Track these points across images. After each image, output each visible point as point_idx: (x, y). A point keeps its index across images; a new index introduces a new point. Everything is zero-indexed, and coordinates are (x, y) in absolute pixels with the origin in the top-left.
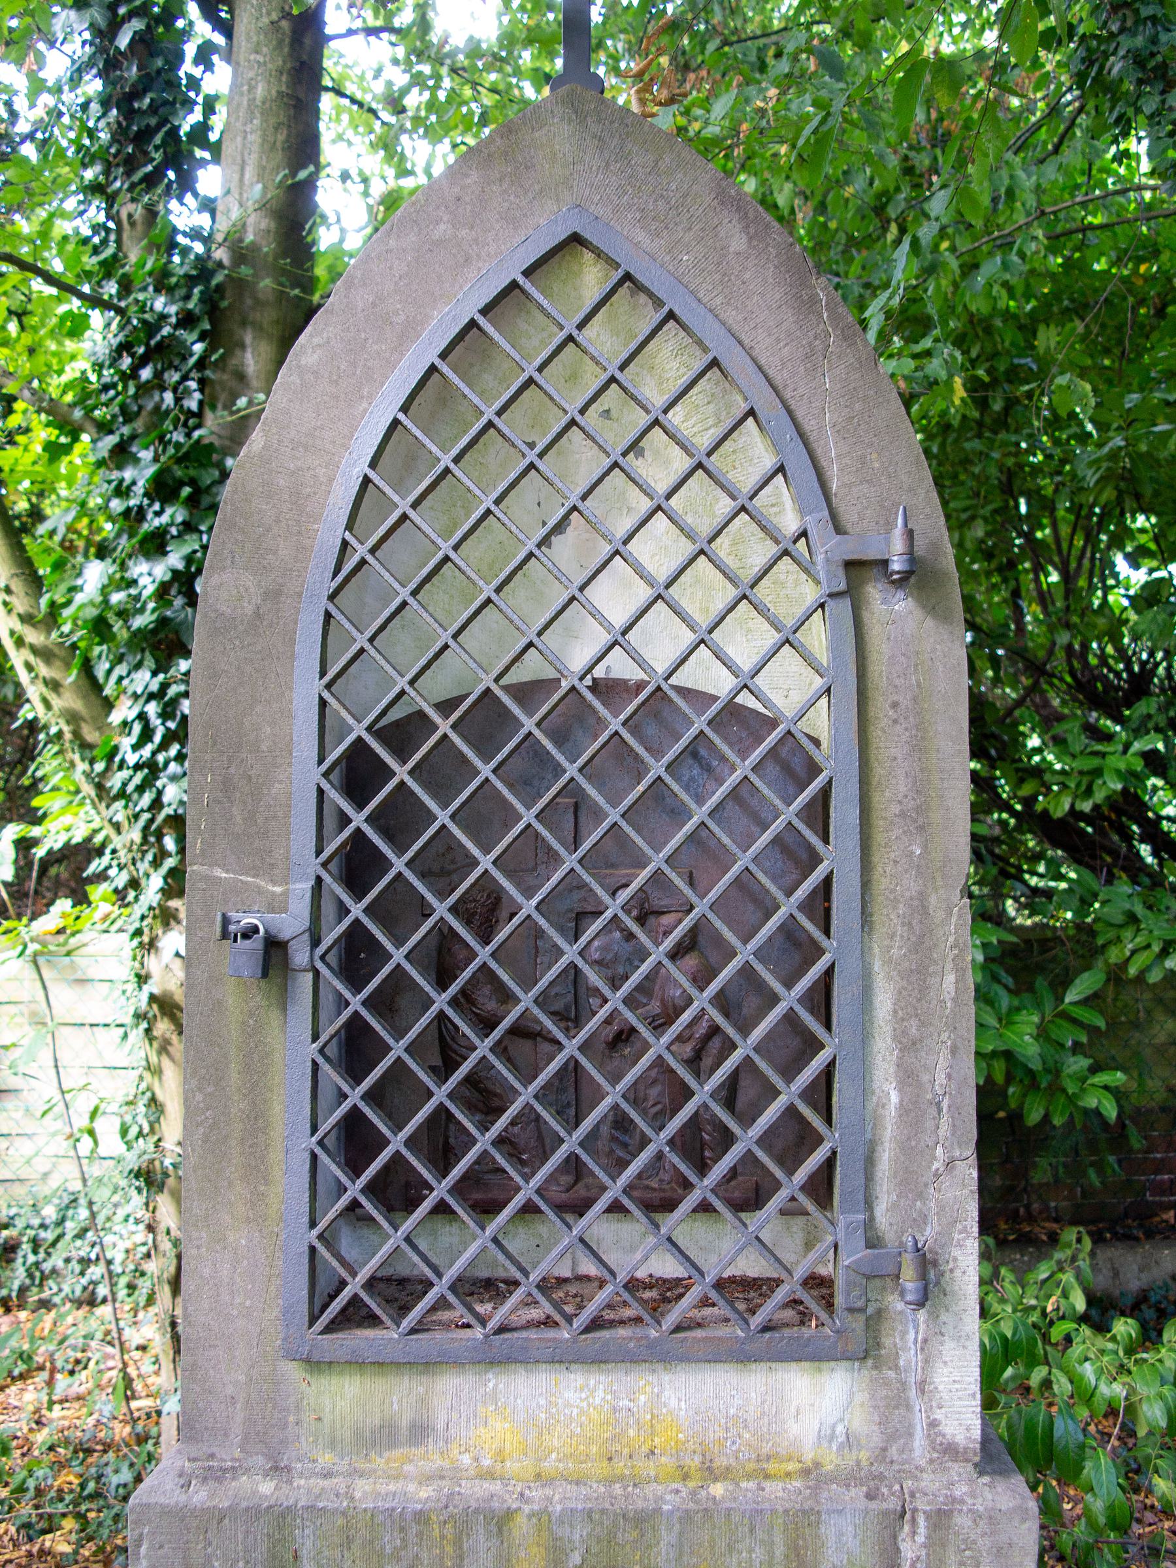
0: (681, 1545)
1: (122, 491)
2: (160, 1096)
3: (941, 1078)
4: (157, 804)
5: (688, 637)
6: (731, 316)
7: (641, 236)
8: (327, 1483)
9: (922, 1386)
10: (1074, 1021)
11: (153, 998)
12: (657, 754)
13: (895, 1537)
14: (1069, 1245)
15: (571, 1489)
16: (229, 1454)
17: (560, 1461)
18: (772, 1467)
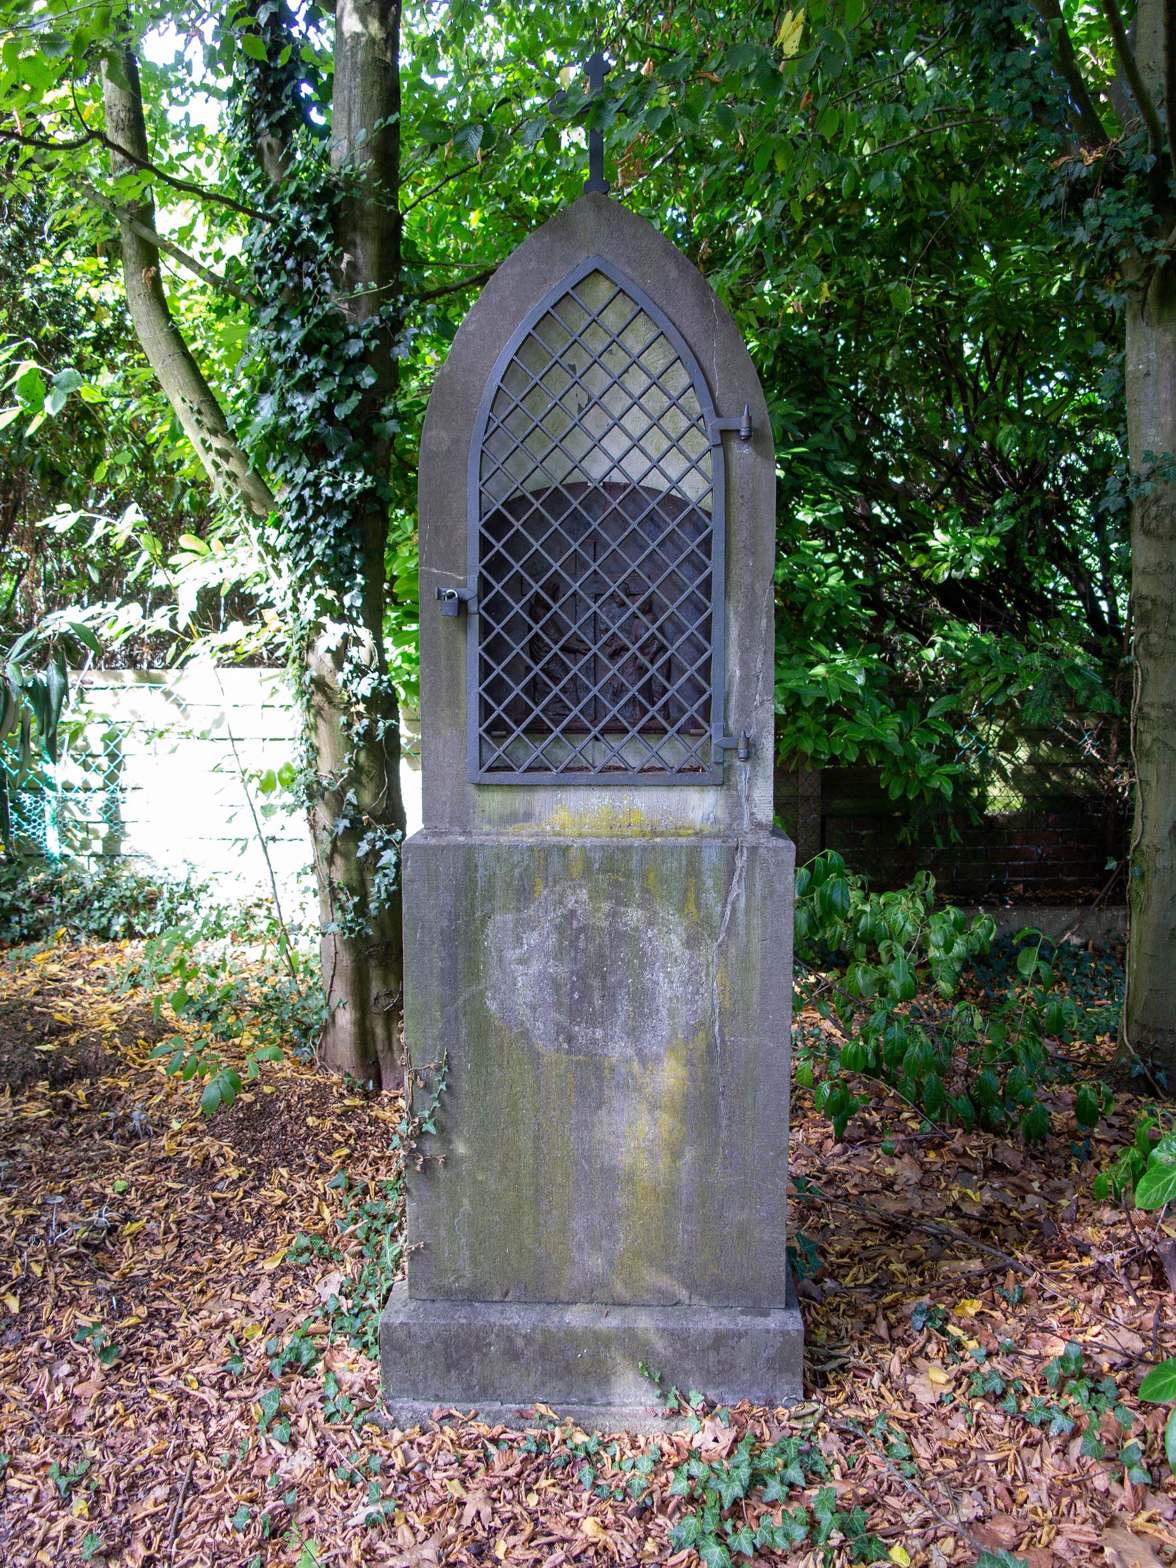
1: (280, 347)
3: (759, 665)
4: (310, 556)
5: (649, 464)
6: (670, 310)
7: (628, 270)
9: (748, 798)
11: (312, 680)
12: (634, 519)
16: (444, 826)
18: (682, 831)
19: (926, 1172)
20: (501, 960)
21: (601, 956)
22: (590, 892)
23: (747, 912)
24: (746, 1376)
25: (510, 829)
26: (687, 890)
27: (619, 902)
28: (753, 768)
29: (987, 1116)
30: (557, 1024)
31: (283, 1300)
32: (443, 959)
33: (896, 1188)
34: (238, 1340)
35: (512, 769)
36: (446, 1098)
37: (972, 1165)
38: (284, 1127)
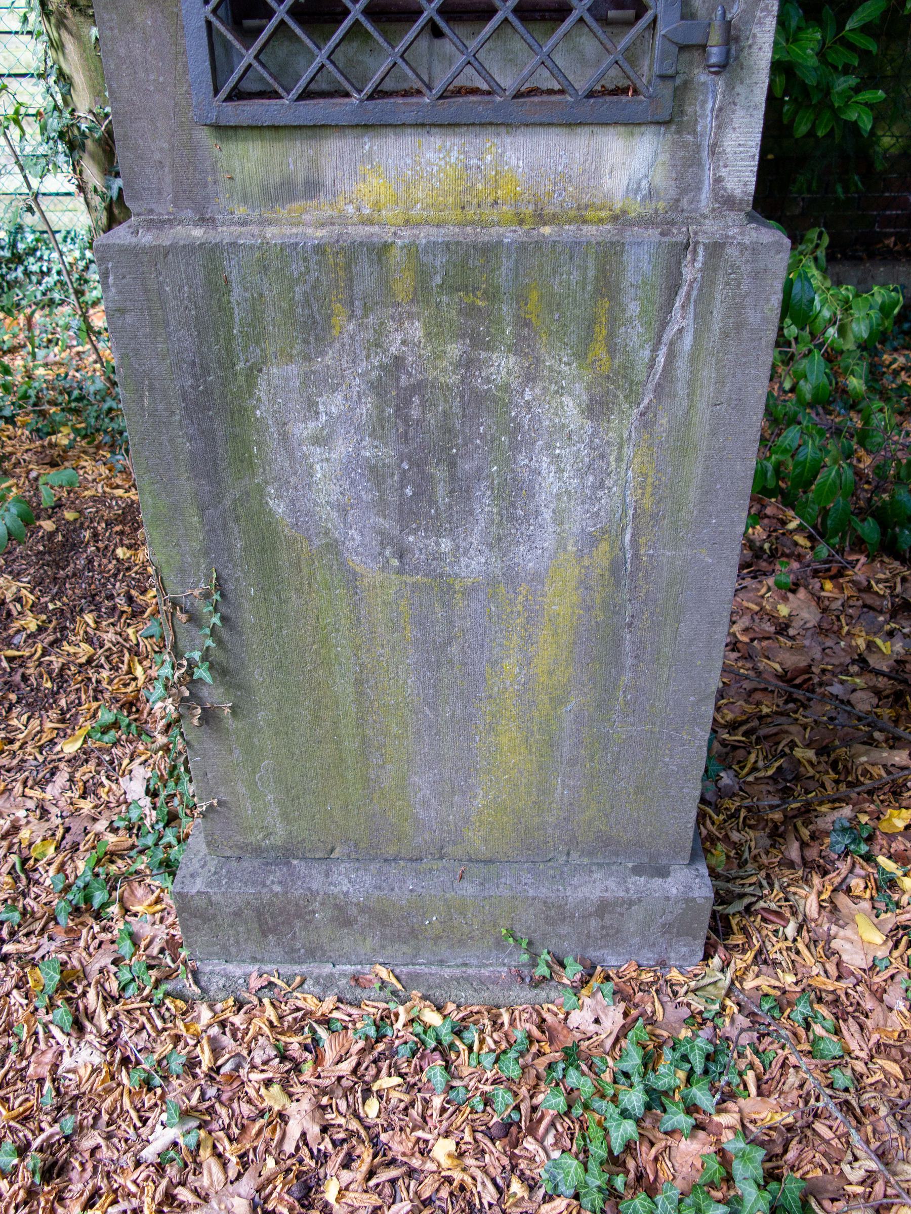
0: (517, 268)
2: (66, 69)
8: (244, 229)
10: (851, 47)
13: (679, 263)
14: (811, 241)
15: (433, 231)
17: (423, 210)
18: (589, 214)
19: (825, 610)
20: (285, 437)
21: (448, 430)
22: (426, 325)
23: (693, 359)
24: (636, 940)
25: (283, 213)
26: (592, 322)
27: (477, 342)
28: (730, 87)
29: (895, 539)
30: (381, 533)
31: (83, 797)
32: (191, 439)
33: (792, 632)
34: (24, 861)
35: (275, 95)
36: (225, 634)
37: (877, 603)
38: (90, 561)
